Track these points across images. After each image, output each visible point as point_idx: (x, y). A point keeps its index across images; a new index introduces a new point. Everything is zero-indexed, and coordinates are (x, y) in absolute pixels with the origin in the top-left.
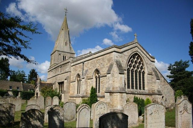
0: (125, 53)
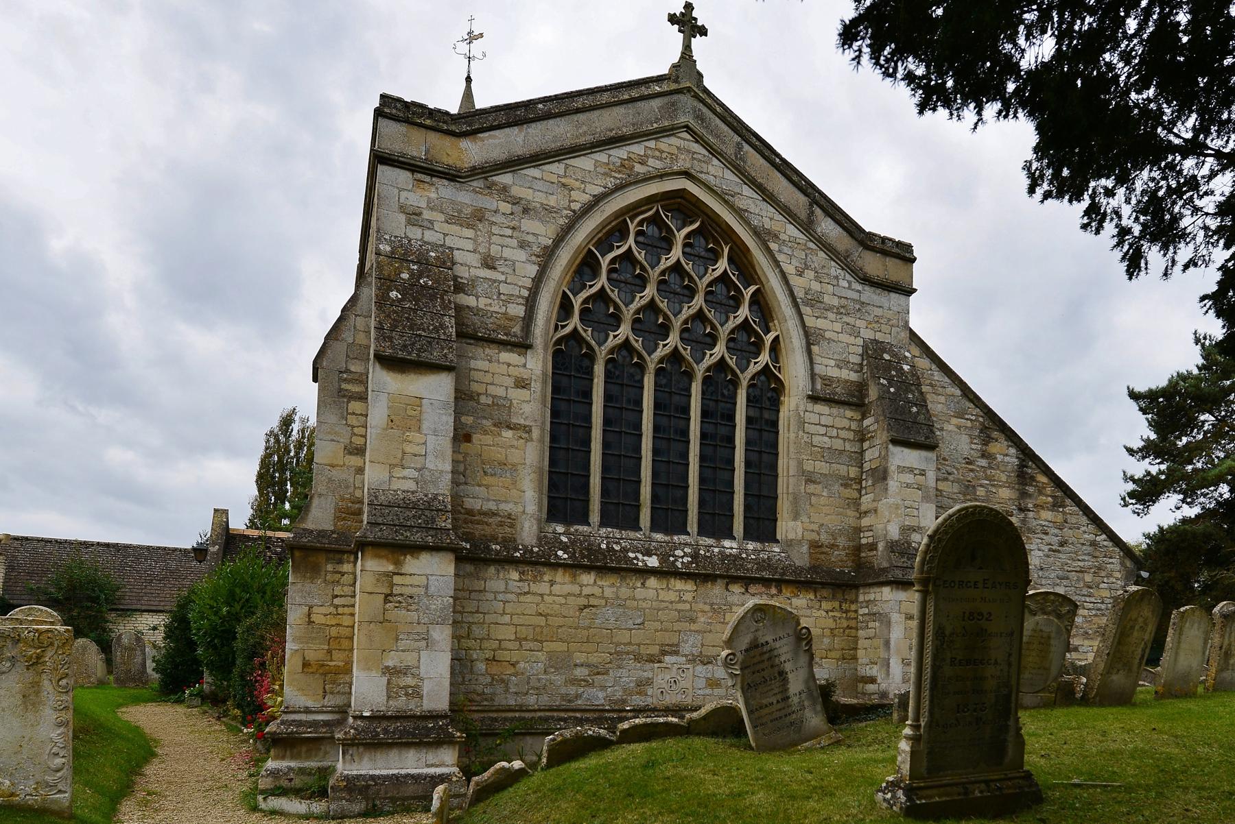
0: (529, 185)
